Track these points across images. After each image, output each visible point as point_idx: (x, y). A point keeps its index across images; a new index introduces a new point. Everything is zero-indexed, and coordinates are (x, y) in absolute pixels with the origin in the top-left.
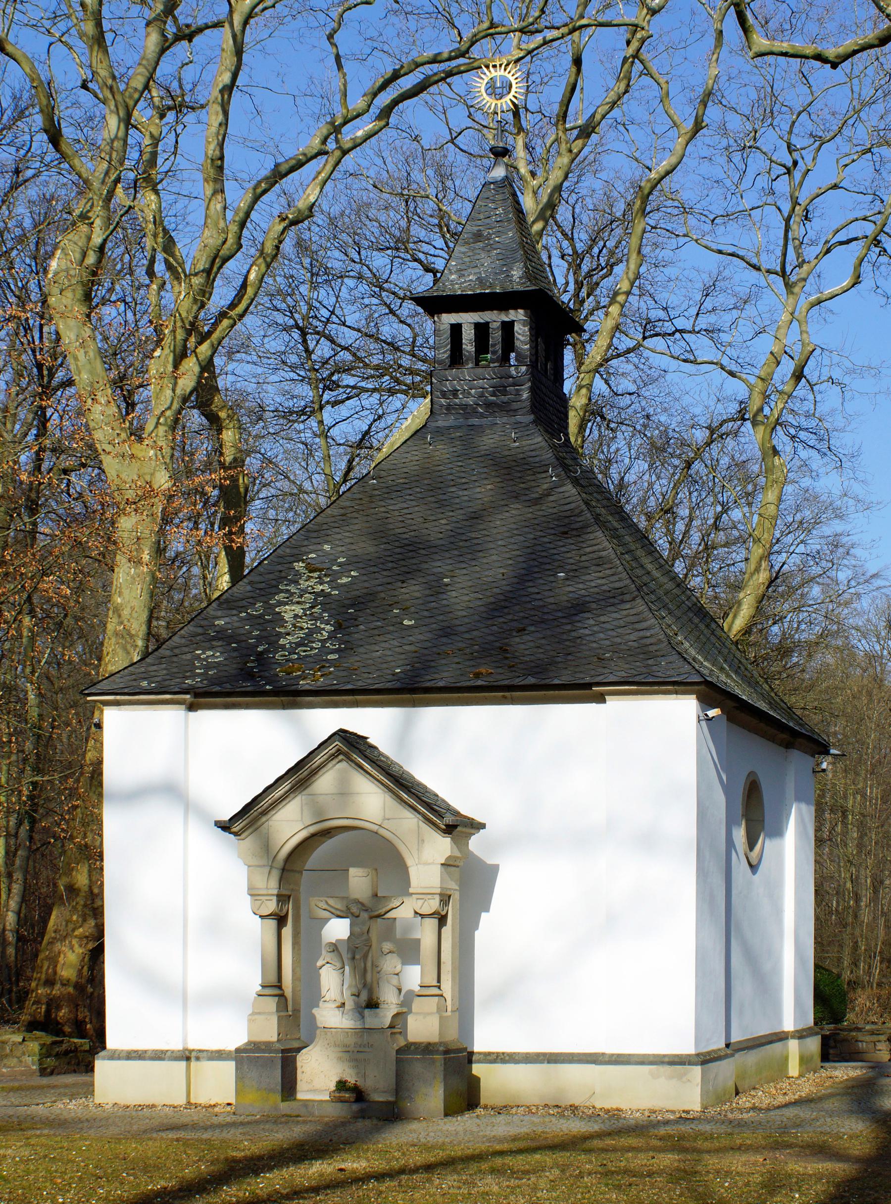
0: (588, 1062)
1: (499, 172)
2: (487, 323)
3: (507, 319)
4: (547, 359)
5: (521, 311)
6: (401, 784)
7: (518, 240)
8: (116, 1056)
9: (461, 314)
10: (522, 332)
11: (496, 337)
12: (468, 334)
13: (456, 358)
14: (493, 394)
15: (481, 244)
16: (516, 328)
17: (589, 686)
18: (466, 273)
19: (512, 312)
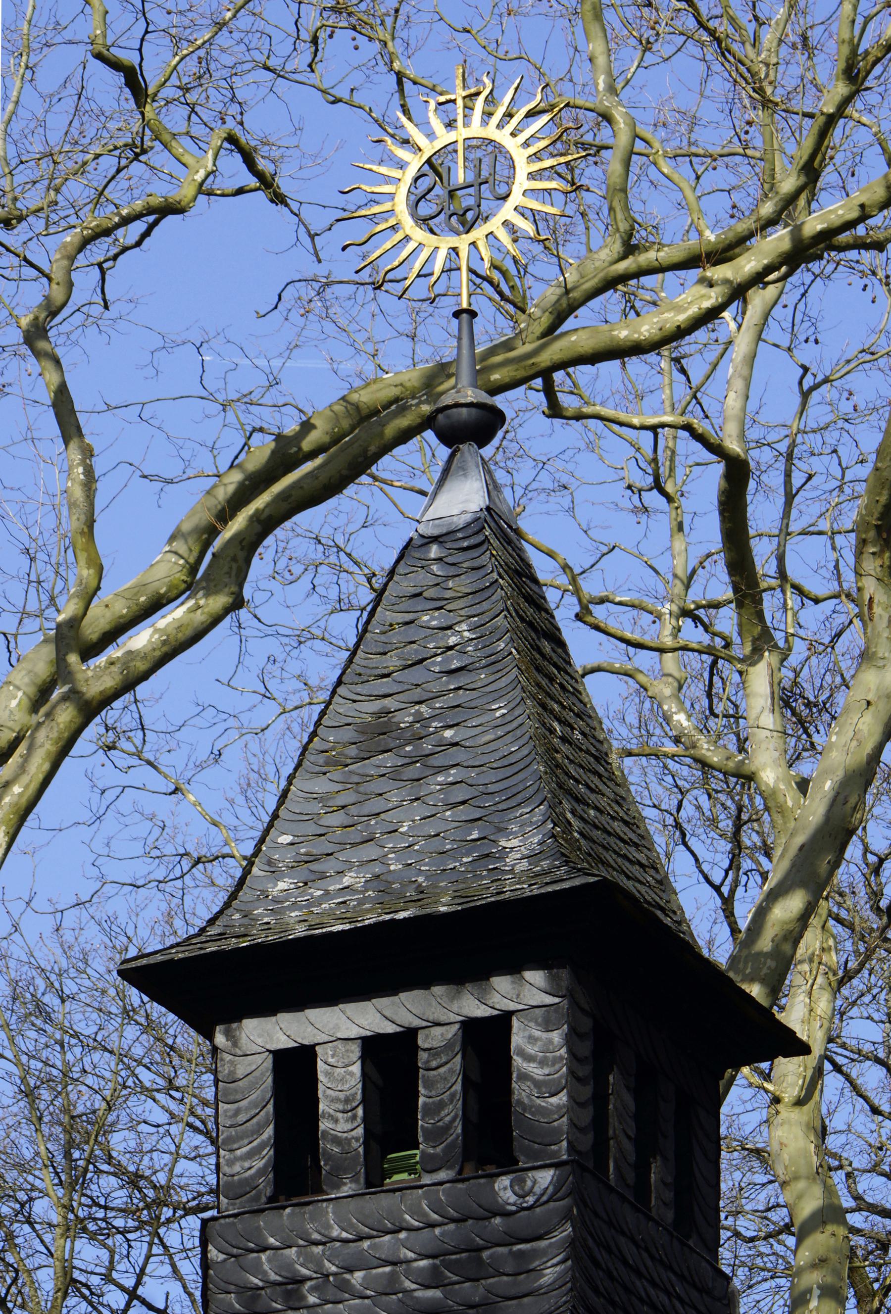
1: (463, 499)
2: (409, 1035)
3: (482, 1011)
4: (646, 1147)
5: (536, 977)
7: (531, 726)
9: (313, 1014)
10: (539, 1053)
11: (441, 1090)
12: (340, 1080)
13: (298, 1166)
14: (432, 1280)
15: (388, 760)
16: (517, 1039)
18: (329, 866)
19: (502, 983)
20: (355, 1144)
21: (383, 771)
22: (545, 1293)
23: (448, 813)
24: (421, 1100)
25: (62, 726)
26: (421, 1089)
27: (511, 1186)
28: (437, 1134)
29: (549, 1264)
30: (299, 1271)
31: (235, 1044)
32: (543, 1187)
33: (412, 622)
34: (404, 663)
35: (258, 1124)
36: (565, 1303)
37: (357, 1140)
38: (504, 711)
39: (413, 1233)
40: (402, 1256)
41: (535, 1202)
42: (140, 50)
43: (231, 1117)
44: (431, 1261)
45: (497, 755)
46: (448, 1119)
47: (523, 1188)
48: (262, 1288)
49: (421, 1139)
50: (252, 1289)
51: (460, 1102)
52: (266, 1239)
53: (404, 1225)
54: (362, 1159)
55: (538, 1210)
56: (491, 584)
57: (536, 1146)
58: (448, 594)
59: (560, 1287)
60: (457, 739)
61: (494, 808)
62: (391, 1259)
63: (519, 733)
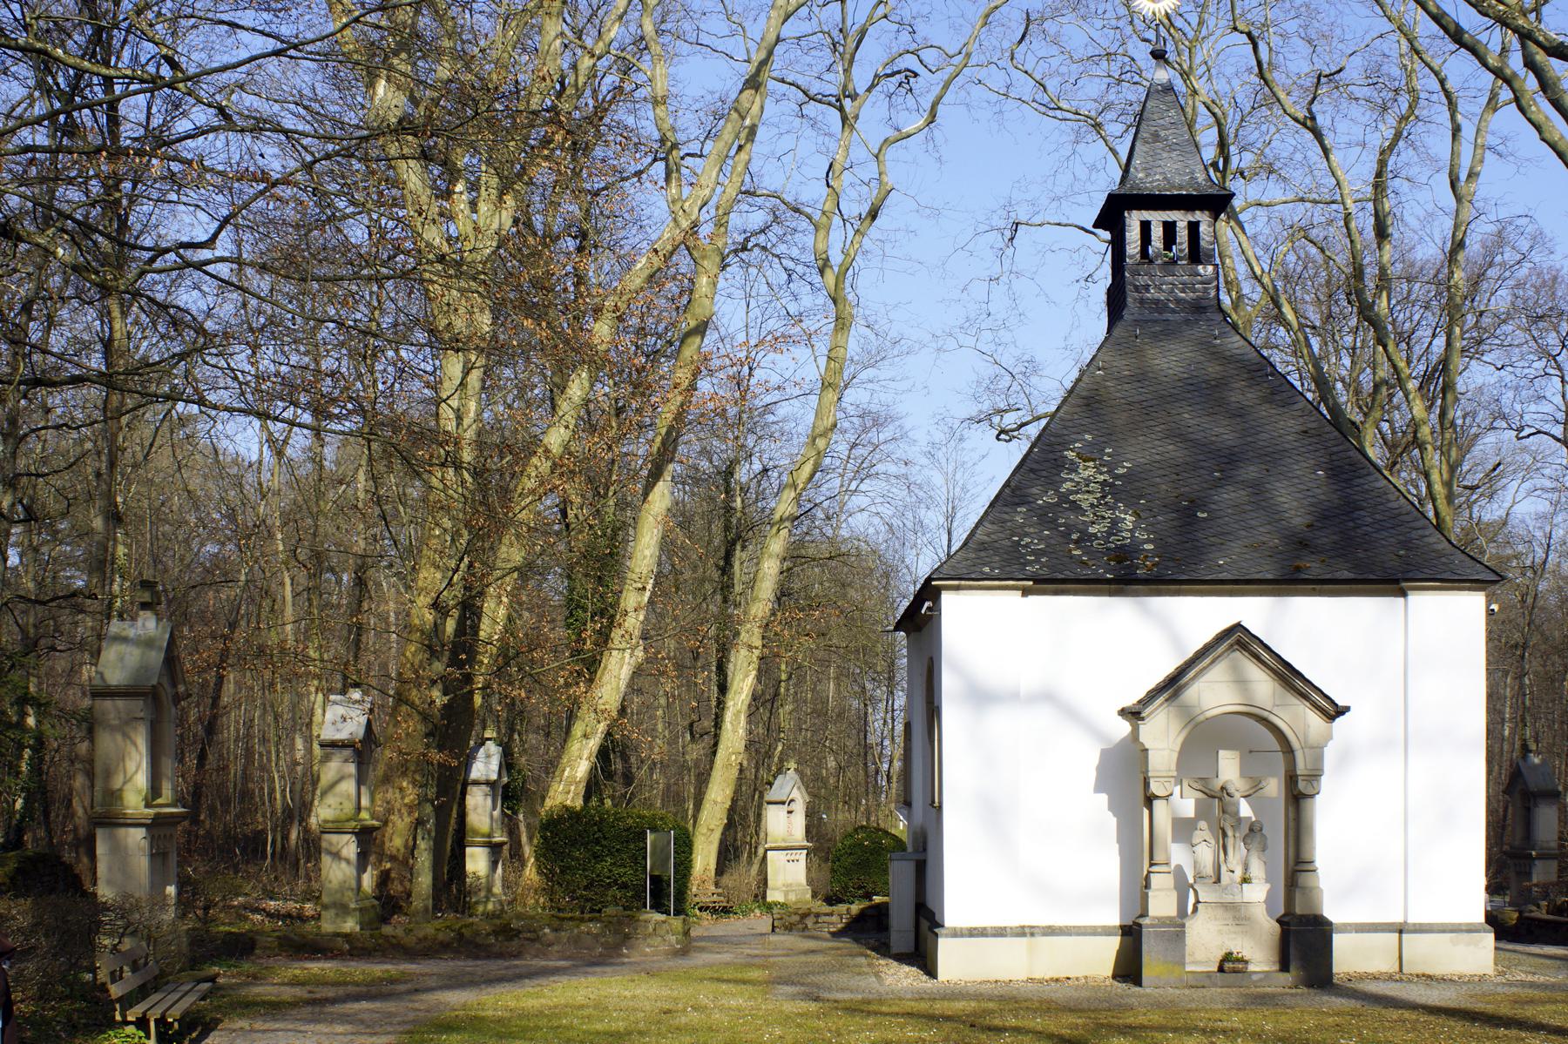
0: (1369, 931)
6: (1288, 676)
8: (956, 933)
12: (1157, 233)
17: (1397, 581)
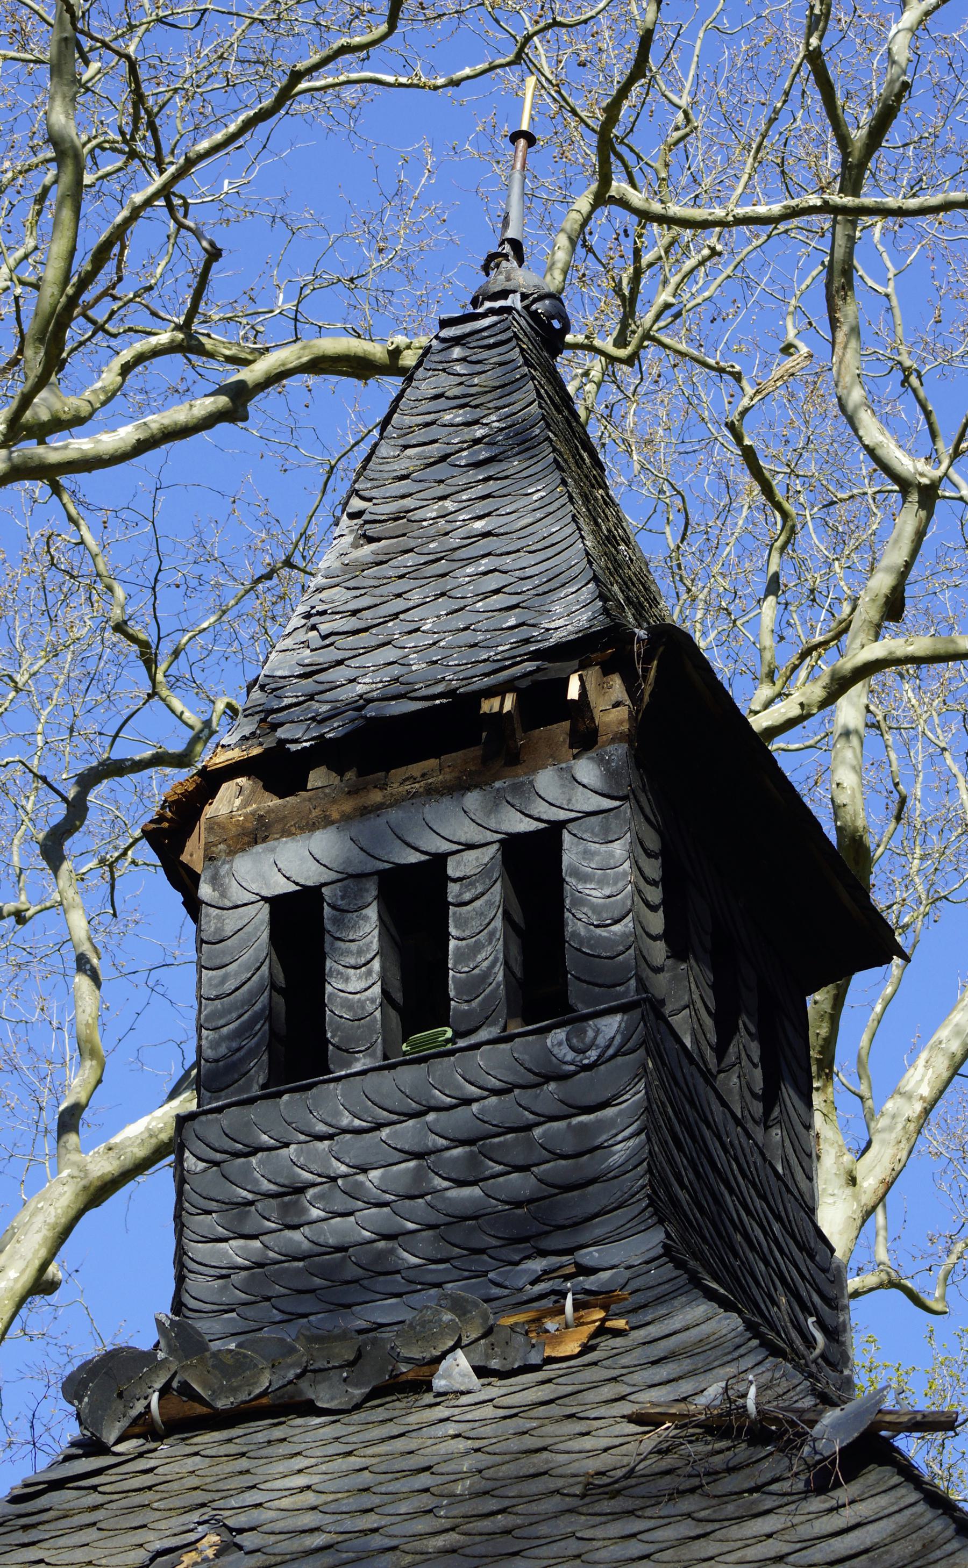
3: (525, 825)
11: (477, 942)
20: (370, 1007)
21: (403, 571)
22: (616, 1177)
23: (480, 604)
24: (452, 944)
25: (59, 1211)
26: (452, 930)
27: (567, 1040)
28: (475, 985)
29: (620, 1137)
30: (299, 1175)
31: (223, 895)
32: (608, 1037)
33: (433, 423)
34: (426, 461)
35: (250, 991)
36: (643, 1187)
37: (373, 1001)
38: (543, 494)
39: (443, 1114)
40: (430, 1144)
41: (599, 1057)
42: (154, 588)
43: (216, 986)
44: (467, 1149)
45: (536, 538)
46: (486, 964)
47: (583, 1042)
48: (251, 1203)
49: (452, 994)
50: (238, 1204)
51: (501, 942)
52: (258, 1137)
53: (433, 1103)
54: (379, 1026)
55: (602, 1067)
56: (522, 377)
57: (597, 989)
58: (473, 390)
59: (635, 1167)
60: (490, 528)
61: (532, 592)
62: (416, 1149)
63: (559, 514)
